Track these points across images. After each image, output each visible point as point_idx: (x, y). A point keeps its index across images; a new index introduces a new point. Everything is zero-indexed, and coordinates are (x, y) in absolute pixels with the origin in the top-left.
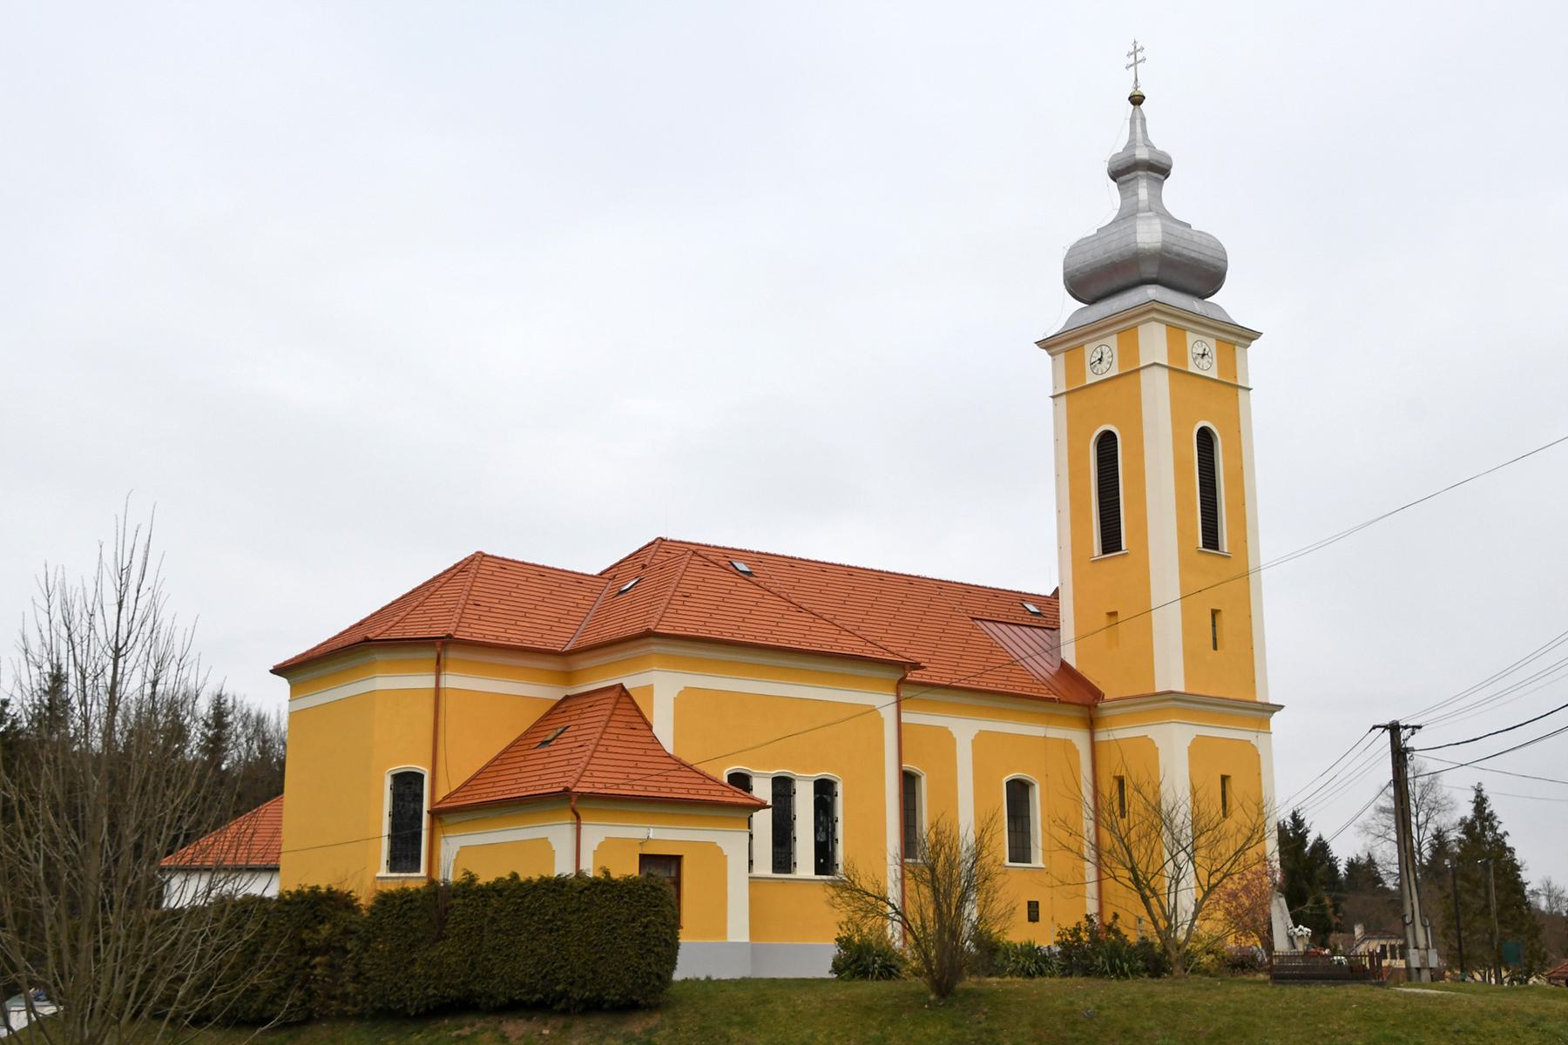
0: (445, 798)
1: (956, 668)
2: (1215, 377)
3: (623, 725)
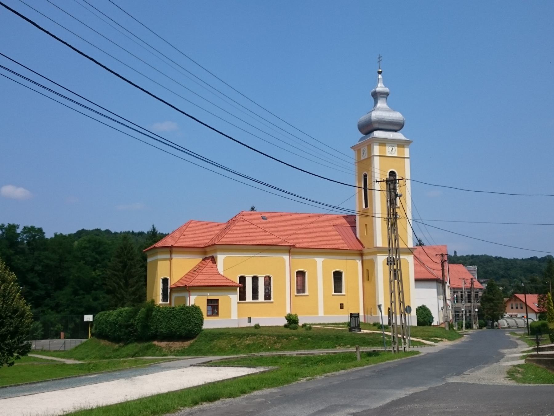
0: (173, 284)
1: (309, 245)
2: (396, 155)
3: (210, 267)
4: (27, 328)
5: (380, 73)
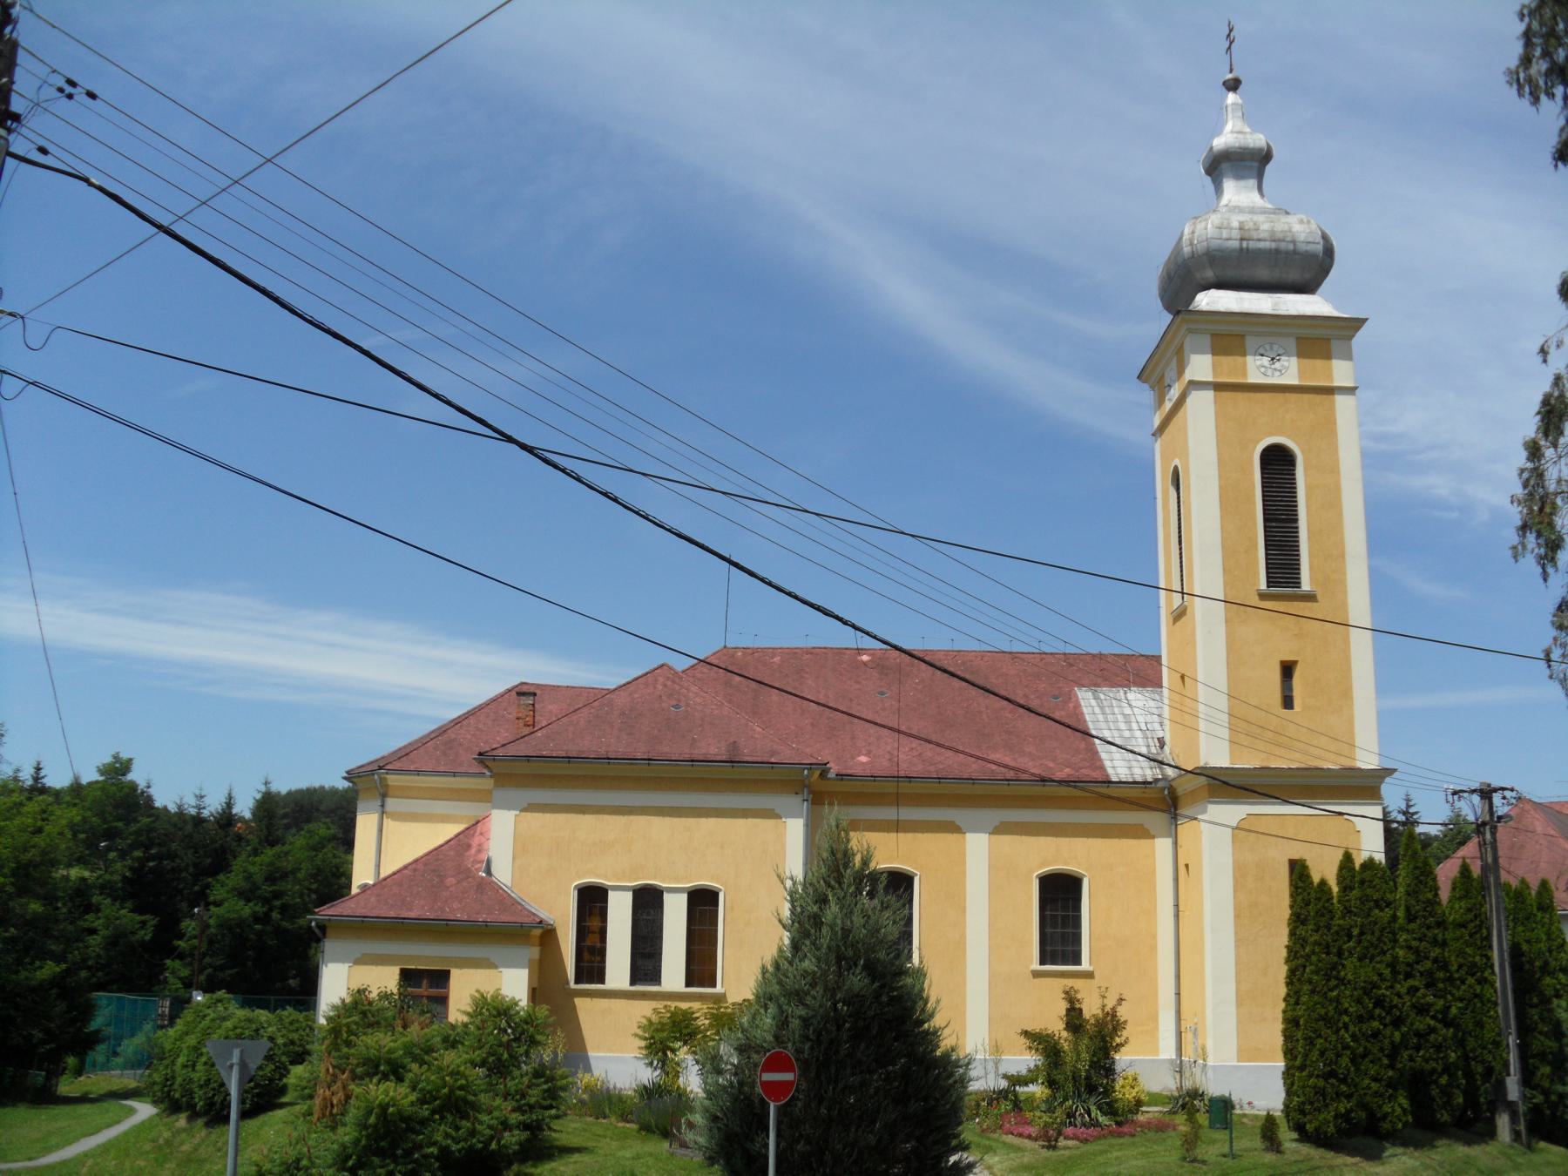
2: (1295, 382)
4: (1466, 1093)
5: (1233, 85)
